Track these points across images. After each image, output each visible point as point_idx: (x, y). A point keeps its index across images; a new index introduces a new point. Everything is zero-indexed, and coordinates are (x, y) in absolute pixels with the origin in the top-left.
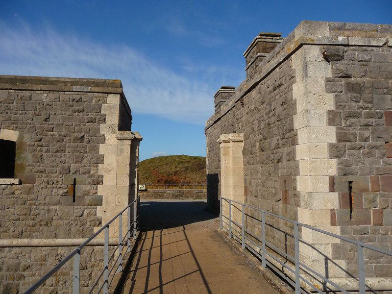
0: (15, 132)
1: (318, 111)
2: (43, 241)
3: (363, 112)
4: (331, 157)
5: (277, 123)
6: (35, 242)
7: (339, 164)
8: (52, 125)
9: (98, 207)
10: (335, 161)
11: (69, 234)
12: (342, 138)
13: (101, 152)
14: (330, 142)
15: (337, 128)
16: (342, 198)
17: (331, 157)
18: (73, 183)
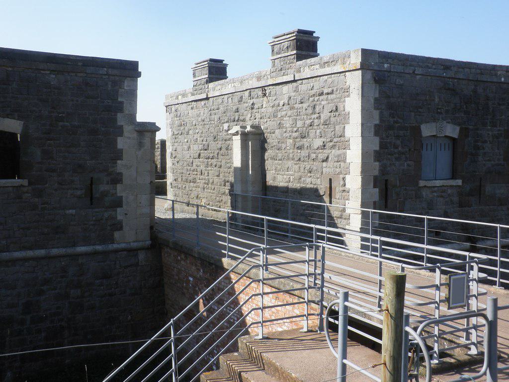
0: (19, 121)
1: (369, 125)
2: (62, 251)
3: (397, 125)
4: (375, 161)
5: (322, 127)
6: (55, 251)
7: (380, 166)
8: (64, 113)
9: (119, 210)
10: (377, 163)
11: (87, 241)
12: (382, 145)
13: (120, 146)
14: (375, 149)
15: (380, 138)
16: (380, 192)
17: (375, 161)
18: (89, 182)
